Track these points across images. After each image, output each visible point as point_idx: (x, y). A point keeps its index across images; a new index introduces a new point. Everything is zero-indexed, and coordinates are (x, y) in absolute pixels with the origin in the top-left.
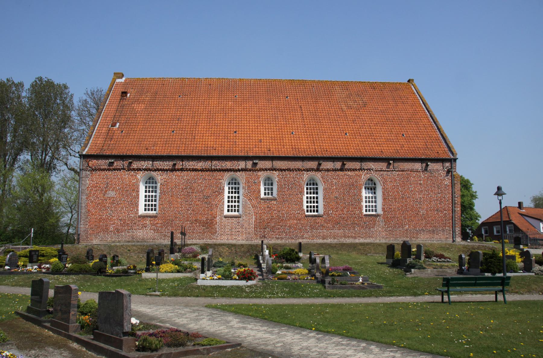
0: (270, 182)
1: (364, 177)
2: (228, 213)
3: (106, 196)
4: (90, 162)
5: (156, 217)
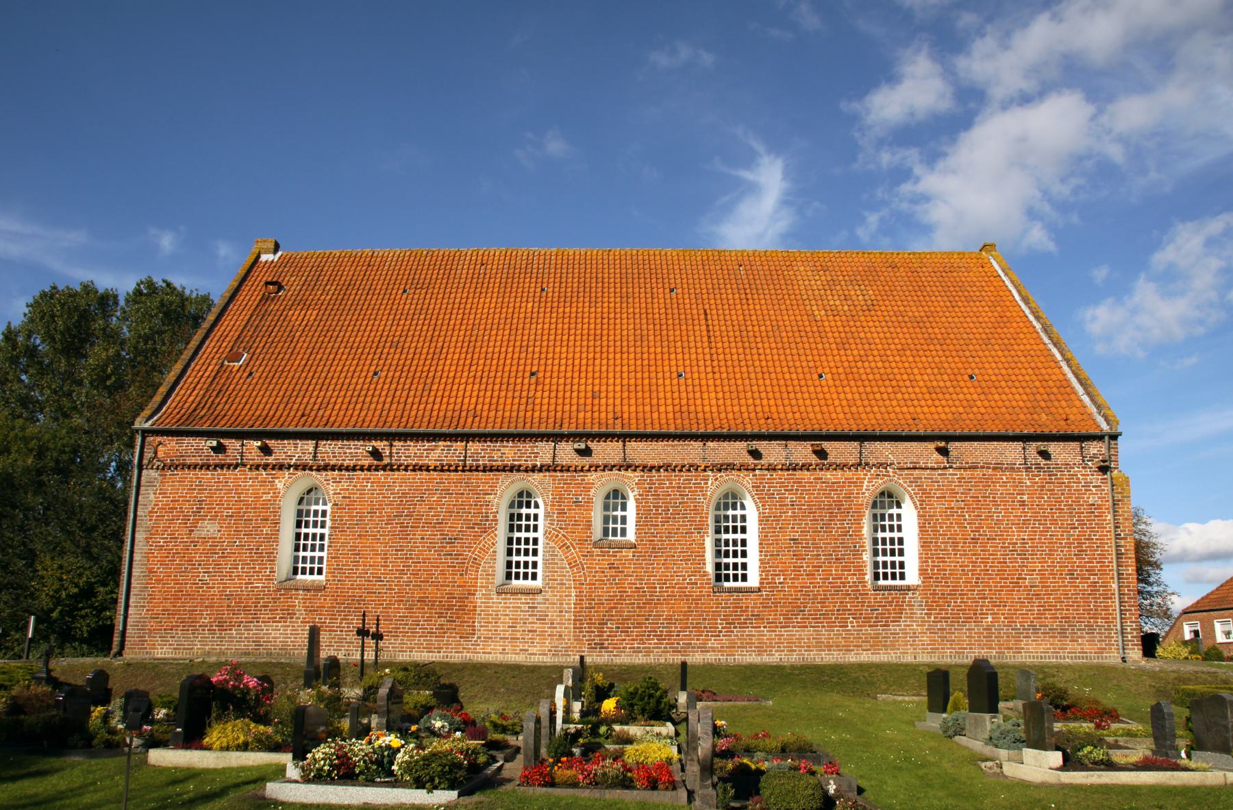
1: (869, 485)
3: (196, 534)
4: (160, 448)
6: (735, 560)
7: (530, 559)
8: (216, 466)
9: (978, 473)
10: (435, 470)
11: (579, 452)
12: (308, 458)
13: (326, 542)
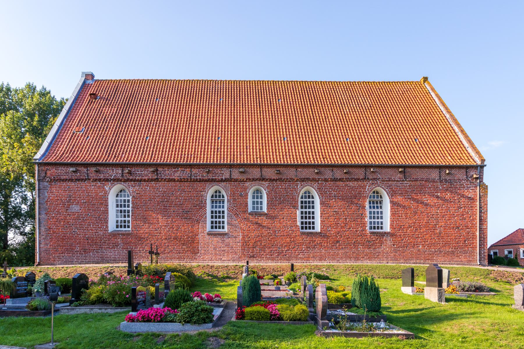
0: (259, 195)
2: (212, 230)
3: (69, 211)
5: (128, 234)
6: (310, 220)
7: (221, 220)
8: (76, 180)
9: (418, 183)
11: (241, 172)
12: (119, 176)
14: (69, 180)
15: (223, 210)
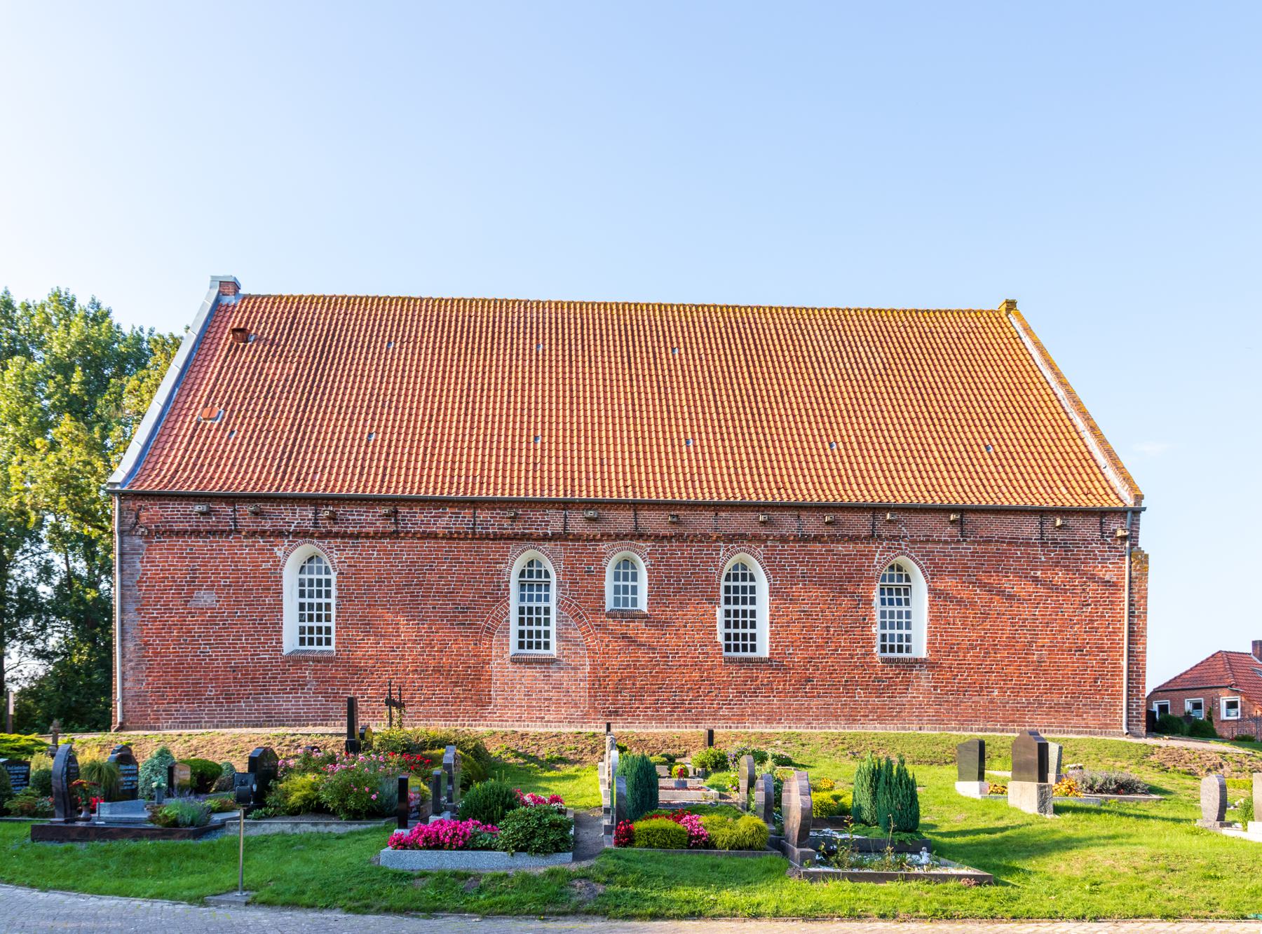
3: (192, 604)
7: (324, 624)
8: (208, 532)
9: (993, 547)
10: (442, 538)
11: (590, 520)
12: (308, 525)
13: (333, 613)
14: (193, 532)
15: (546, 605)
